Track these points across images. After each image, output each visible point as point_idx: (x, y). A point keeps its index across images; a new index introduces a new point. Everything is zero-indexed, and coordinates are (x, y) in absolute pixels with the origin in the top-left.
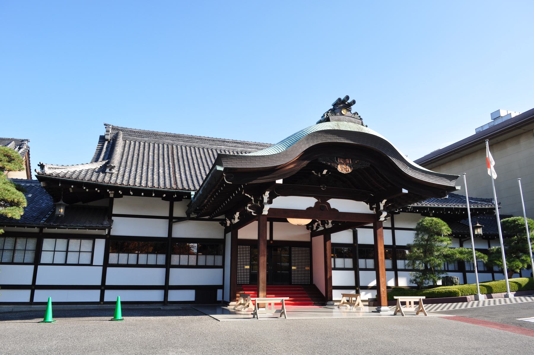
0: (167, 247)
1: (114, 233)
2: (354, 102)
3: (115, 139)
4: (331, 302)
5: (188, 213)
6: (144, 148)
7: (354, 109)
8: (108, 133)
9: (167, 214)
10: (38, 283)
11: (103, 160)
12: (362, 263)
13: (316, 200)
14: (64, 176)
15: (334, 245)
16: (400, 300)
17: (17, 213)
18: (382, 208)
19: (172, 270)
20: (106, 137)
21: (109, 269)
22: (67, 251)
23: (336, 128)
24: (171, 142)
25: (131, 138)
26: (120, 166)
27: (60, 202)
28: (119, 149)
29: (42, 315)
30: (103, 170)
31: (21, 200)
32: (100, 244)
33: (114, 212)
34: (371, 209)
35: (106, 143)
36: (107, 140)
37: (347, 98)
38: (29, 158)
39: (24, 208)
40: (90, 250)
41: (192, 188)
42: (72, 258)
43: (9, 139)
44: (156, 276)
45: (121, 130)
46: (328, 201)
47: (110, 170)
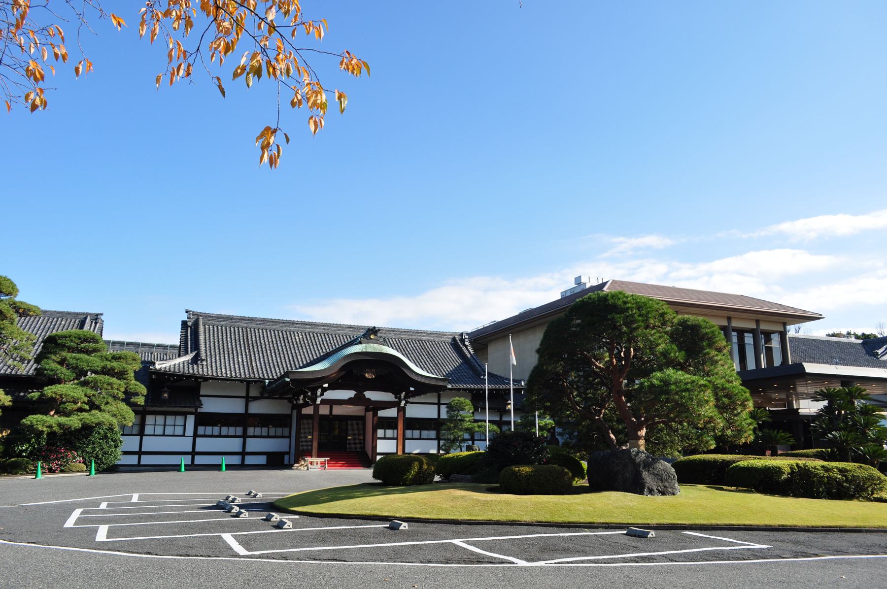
3: (196, 324)
11: (191, 352)
22: (165, 425)
29: (179, 470)
32: (191, 420)
33: (201, 393)
41: (266, 377)
44: (234, 444)
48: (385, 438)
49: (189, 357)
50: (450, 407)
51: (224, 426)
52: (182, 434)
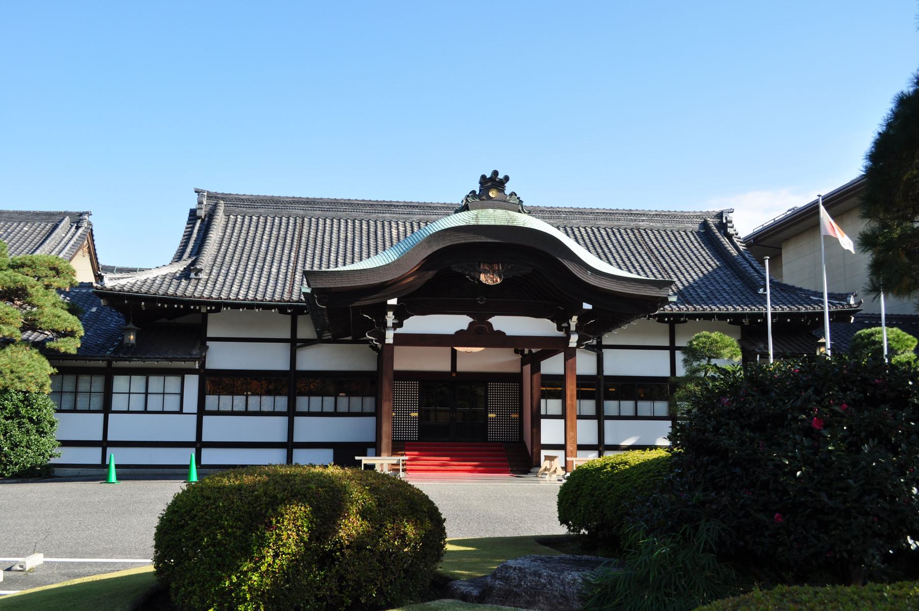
0: (289, 385)
1: (209, 366)
2: (507, 178)
3: (211, 215)
5: (320, 334)
6: (257, 227)
7: (509, 188)
8: (200, 206)
9: (288, 336)
10: (110, 438)
11: (189, 257)
12: (611, 407)
13: (471, 320)
14: (130, 290)
16: (364, 462)
17: (71, 346)
18: (573, 328)
19: (298, 420)
20: (199, 213)
21: (206, 419)
22: (147, 394)
23: (473, 223)
24: (302, 212)
25: (238, 210)
26: (213, 265)
27: (129, 326)
28: (215, 235)
29: (104, 478)
30: (186, 274)
31: (75, 328)
32: (192, 383)
33: (210, 334)
34: (560, 328)
35: (199, 222)
36: (200, 217)
37: (496, 173)
38: (93, 241)
39: (81, 338)
40: (178, 391)
42: (154, 403)
43: (61, 213)
44: (275, 428)
45: (222, 199)
46: (490, 320)
47: (196, 274)
48: (619, 418)
49: (180, 267)
50: (692, 353)
52: (177, 409)
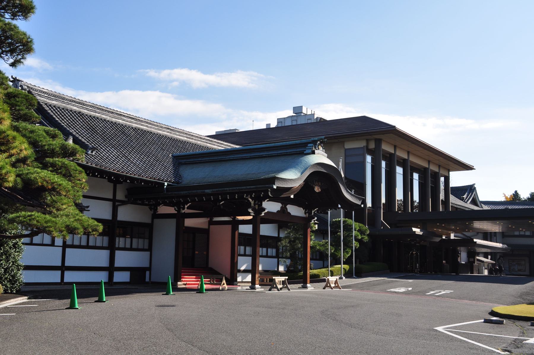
4: (236, 283)
9: (111, 197)
15: (241, 235)
48: (267, 256)
51: (270, 247)
